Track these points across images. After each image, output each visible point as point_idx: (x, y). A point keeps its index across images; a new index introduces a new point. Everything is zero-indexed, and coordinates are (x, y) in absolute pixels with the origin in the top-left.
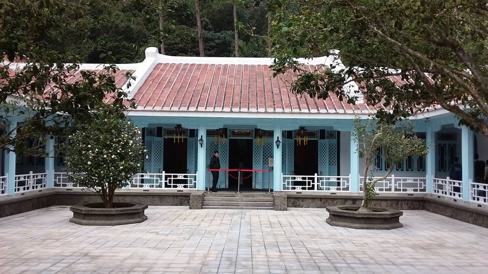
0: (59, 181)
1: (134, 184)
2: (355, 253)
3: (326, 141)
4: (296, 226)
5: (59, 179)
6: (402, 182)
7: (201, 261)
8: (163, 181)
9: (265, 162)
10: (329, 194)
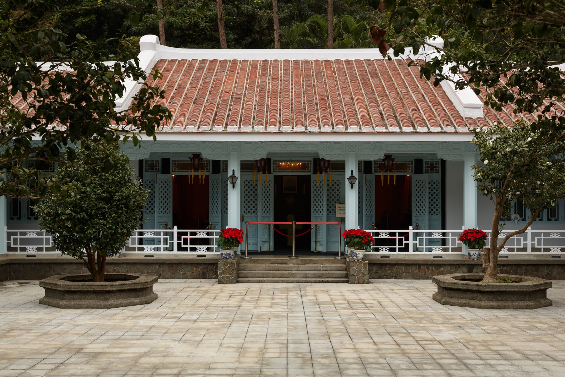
0: (15, 243)
1: (130, 246)
2: (489, 343)
3: (424, 177)
4: (388, 306)
5: (15, 240)
6: (542, 237)
7: (259, 359)
9: (331, 210)
10: (431, 258)
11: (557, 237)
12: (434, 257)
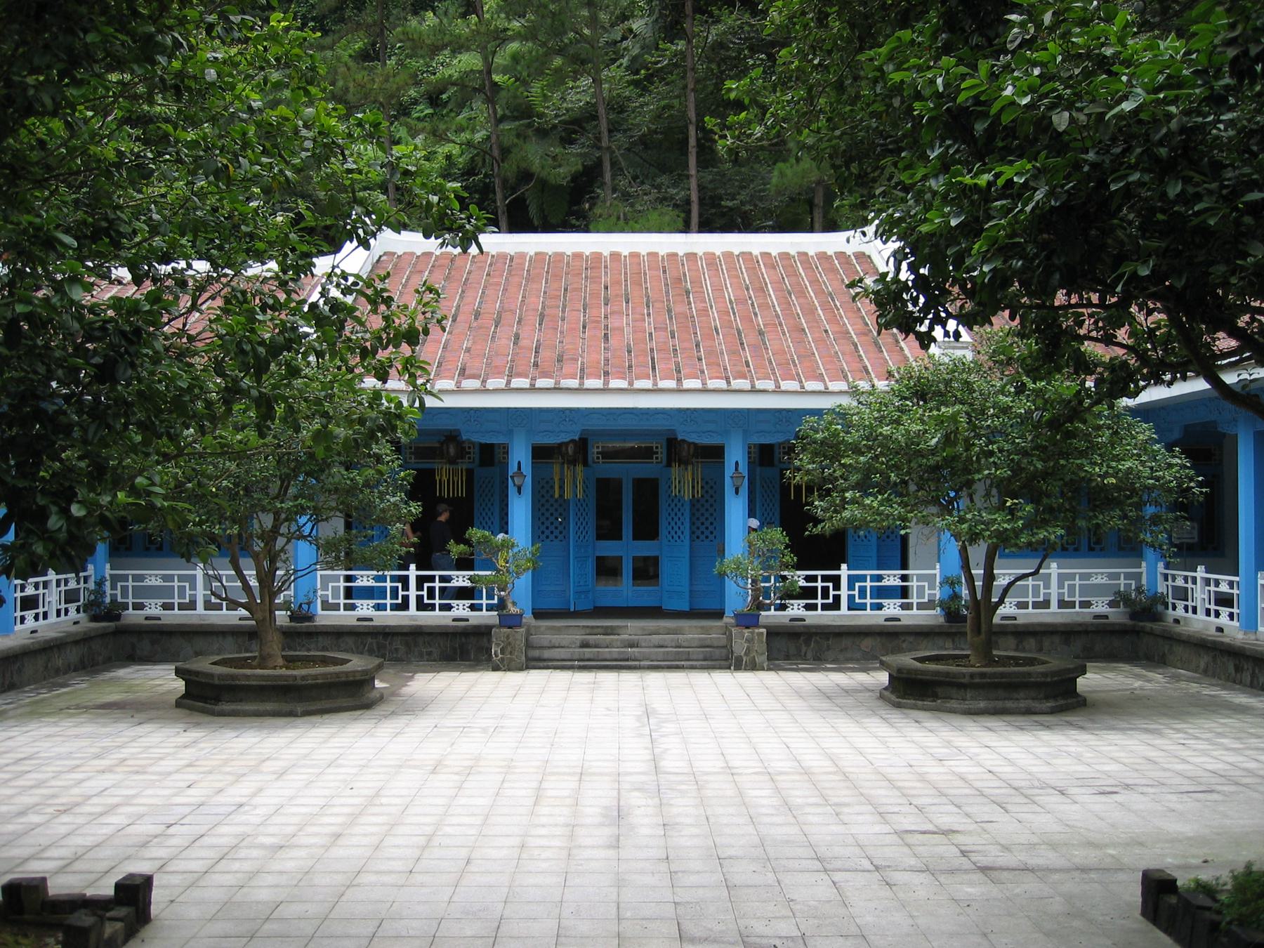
5: (125, 589)
8: (413, 593)
10: (1089, 619)
11: (1103, 581)
12: (886, 620)
